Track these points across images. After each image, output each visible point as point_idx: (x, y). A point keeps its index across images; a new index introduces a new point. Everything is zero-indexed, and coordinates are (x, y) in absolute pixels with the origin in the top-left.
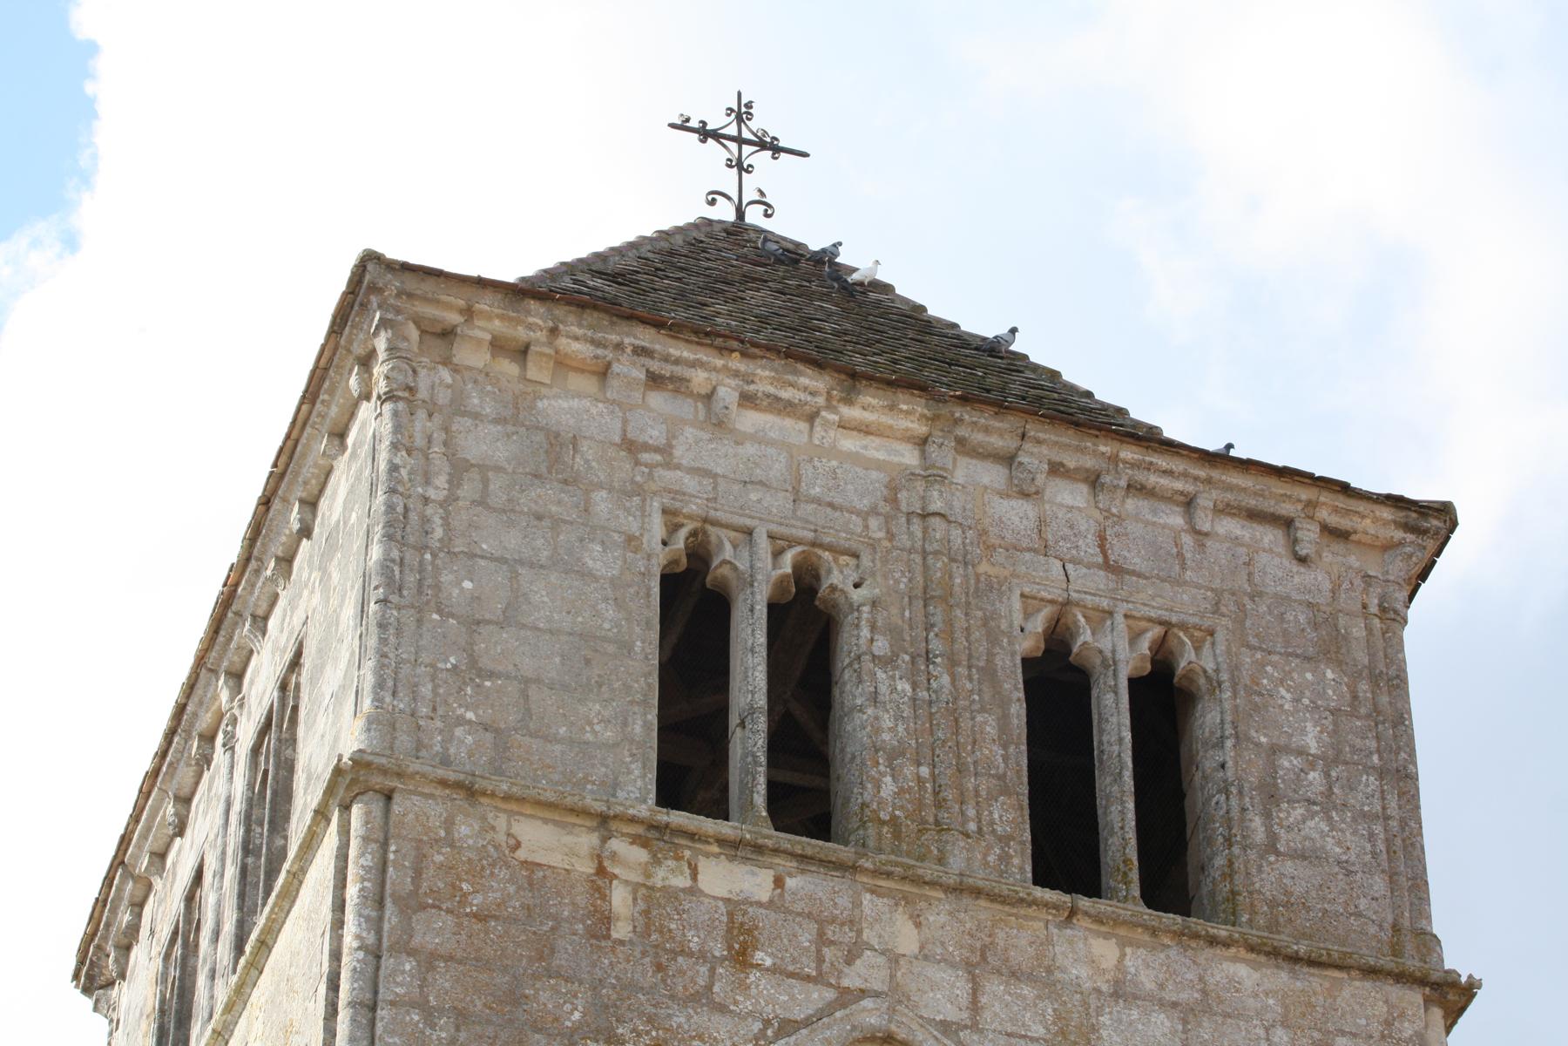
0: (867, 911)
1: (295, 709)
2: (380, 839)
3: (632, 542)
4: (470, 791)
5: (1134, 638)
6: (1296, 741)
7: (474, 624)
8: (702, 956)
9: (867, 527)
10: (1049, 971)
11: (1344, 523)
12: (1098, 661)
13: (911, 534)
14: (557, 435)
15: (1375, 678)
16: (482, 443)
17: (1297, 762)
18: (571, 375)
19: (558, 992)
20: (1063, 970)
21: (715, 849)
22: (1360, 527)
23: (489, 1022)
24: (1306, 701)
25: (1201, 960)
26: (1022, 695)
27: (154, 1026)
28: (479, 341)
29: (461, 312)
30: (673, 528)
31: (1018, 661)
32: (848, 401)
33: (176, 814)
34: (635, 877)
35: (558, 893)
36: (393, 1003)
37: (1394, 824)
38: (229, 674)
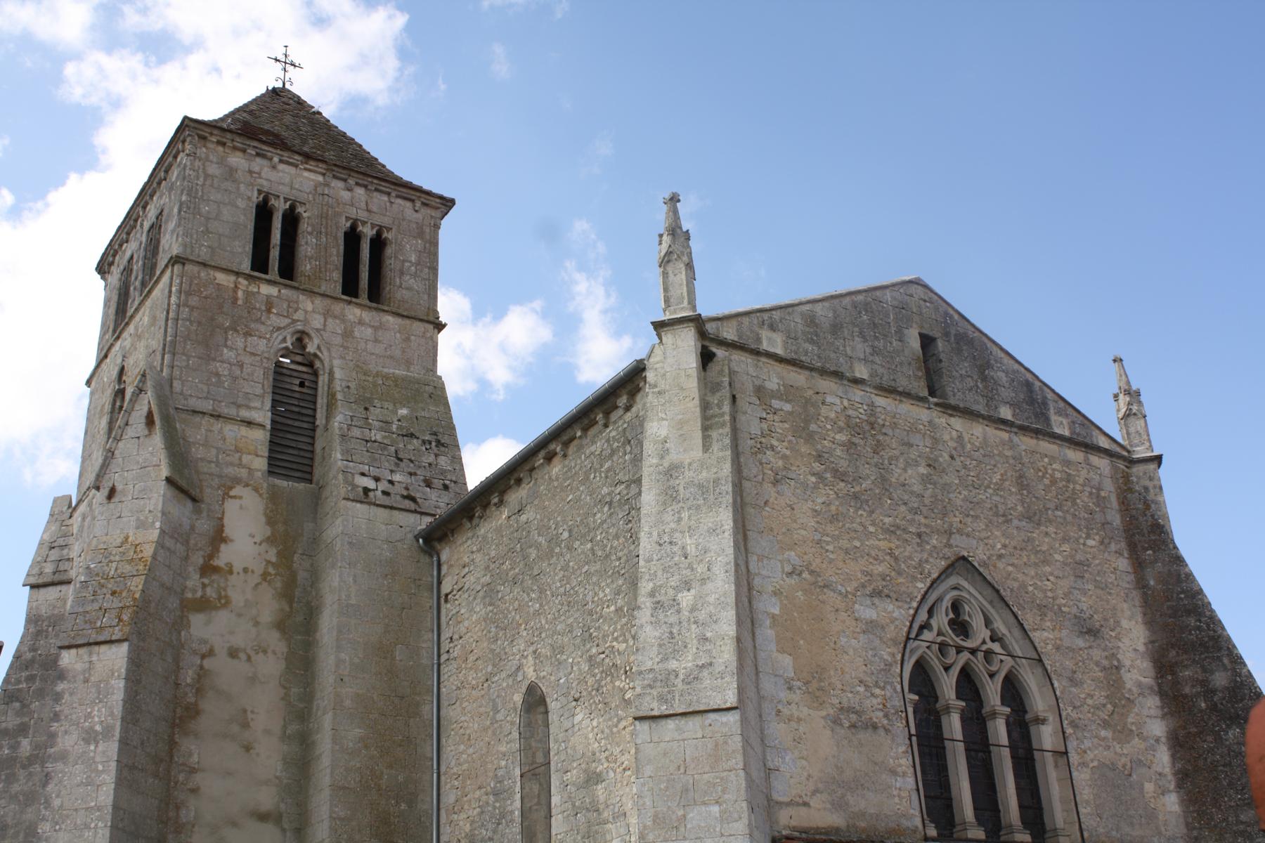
3: (249, 198)
7: (208, 219)
8: (259, 309)
15: (431, 243)
16: (213, 169)
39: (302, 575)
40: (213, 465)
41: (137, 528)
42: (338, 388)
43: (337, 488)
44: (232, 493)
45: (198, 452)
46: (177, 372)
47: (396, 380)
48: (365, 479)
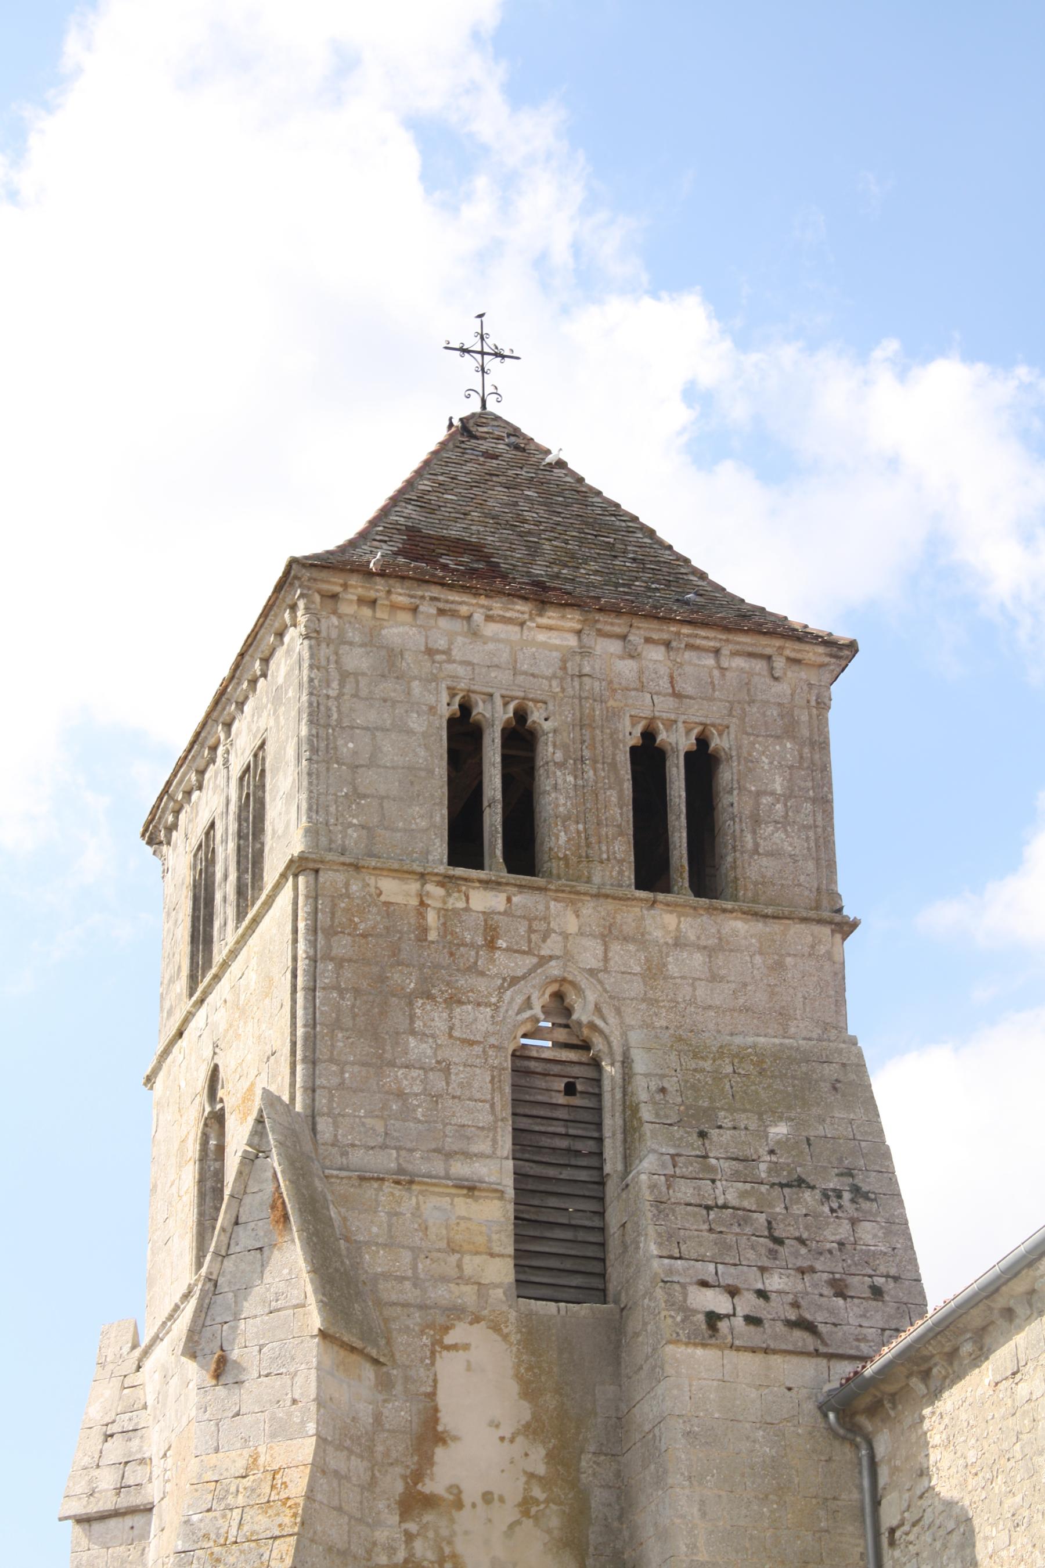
0: (553, 911)
1: (263, 771)
2: (314, 896)
3: (432, 709)
4: (357, 867)
5: (688, 732)
6: (770, 788)
7: (354, 768)
8: (472, 945)
9: (551, 686)
10: (643, 935)
11: (799, 656)
12: (669, 748)
13: (573, 687)
14: (393, 650)
15: (812, 744)
16: (356, 659)
17: (770, 799)
18: (399, 612)
19: (403, 973)
20: (650, 934)
21: (477, 885)
22: (806, 657)
23: (370, 994)
24: (776, 763)
25: (719, 921)
26: (629, 776)
27: (190, 894)
28: (351, 601)
29: (341, 585)
30: (453, 696)
31: (628, 749)
32: (541, 615)
33: (197, 780)
34: (439, 905)
35: (402, 919)
36: (324, 988)
37: (819, 830)
38: (224, 724)
39: (598, 1497)
40: (407, 1284)
41: (273, 1435)
42: (643, 1096)
43: (654, 1316)
44: (449, 1339)
45: (376, 1261)
46: (322, 1101)
47: (760, 1059)
48: (709, 1293)
